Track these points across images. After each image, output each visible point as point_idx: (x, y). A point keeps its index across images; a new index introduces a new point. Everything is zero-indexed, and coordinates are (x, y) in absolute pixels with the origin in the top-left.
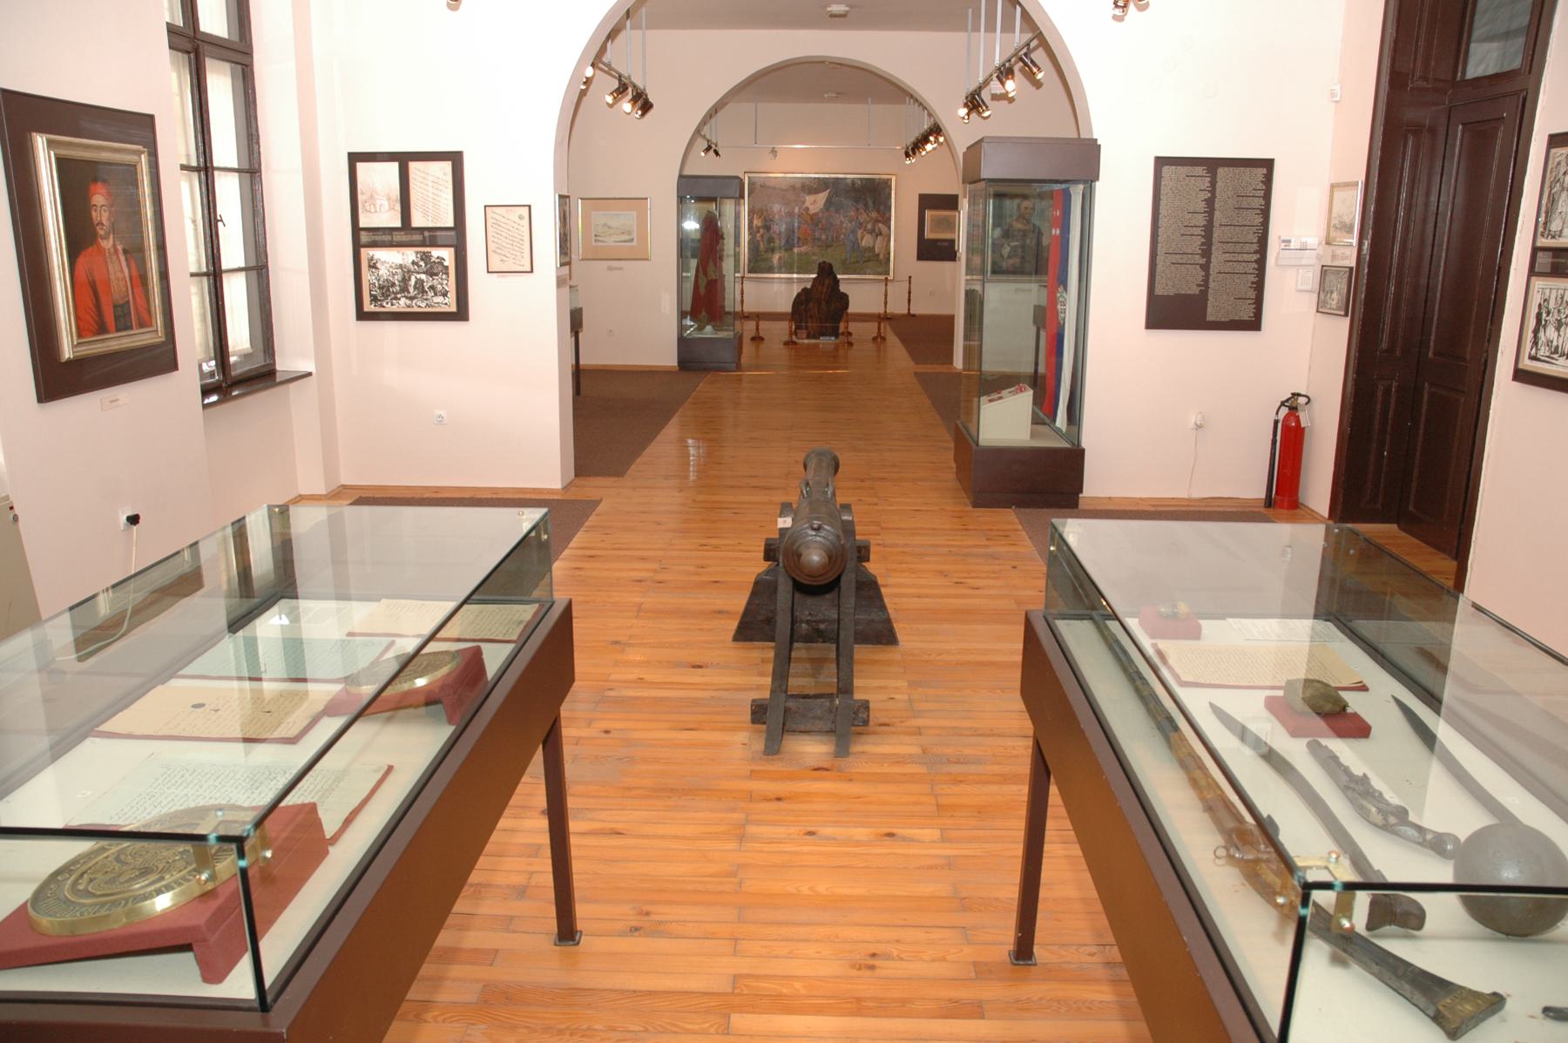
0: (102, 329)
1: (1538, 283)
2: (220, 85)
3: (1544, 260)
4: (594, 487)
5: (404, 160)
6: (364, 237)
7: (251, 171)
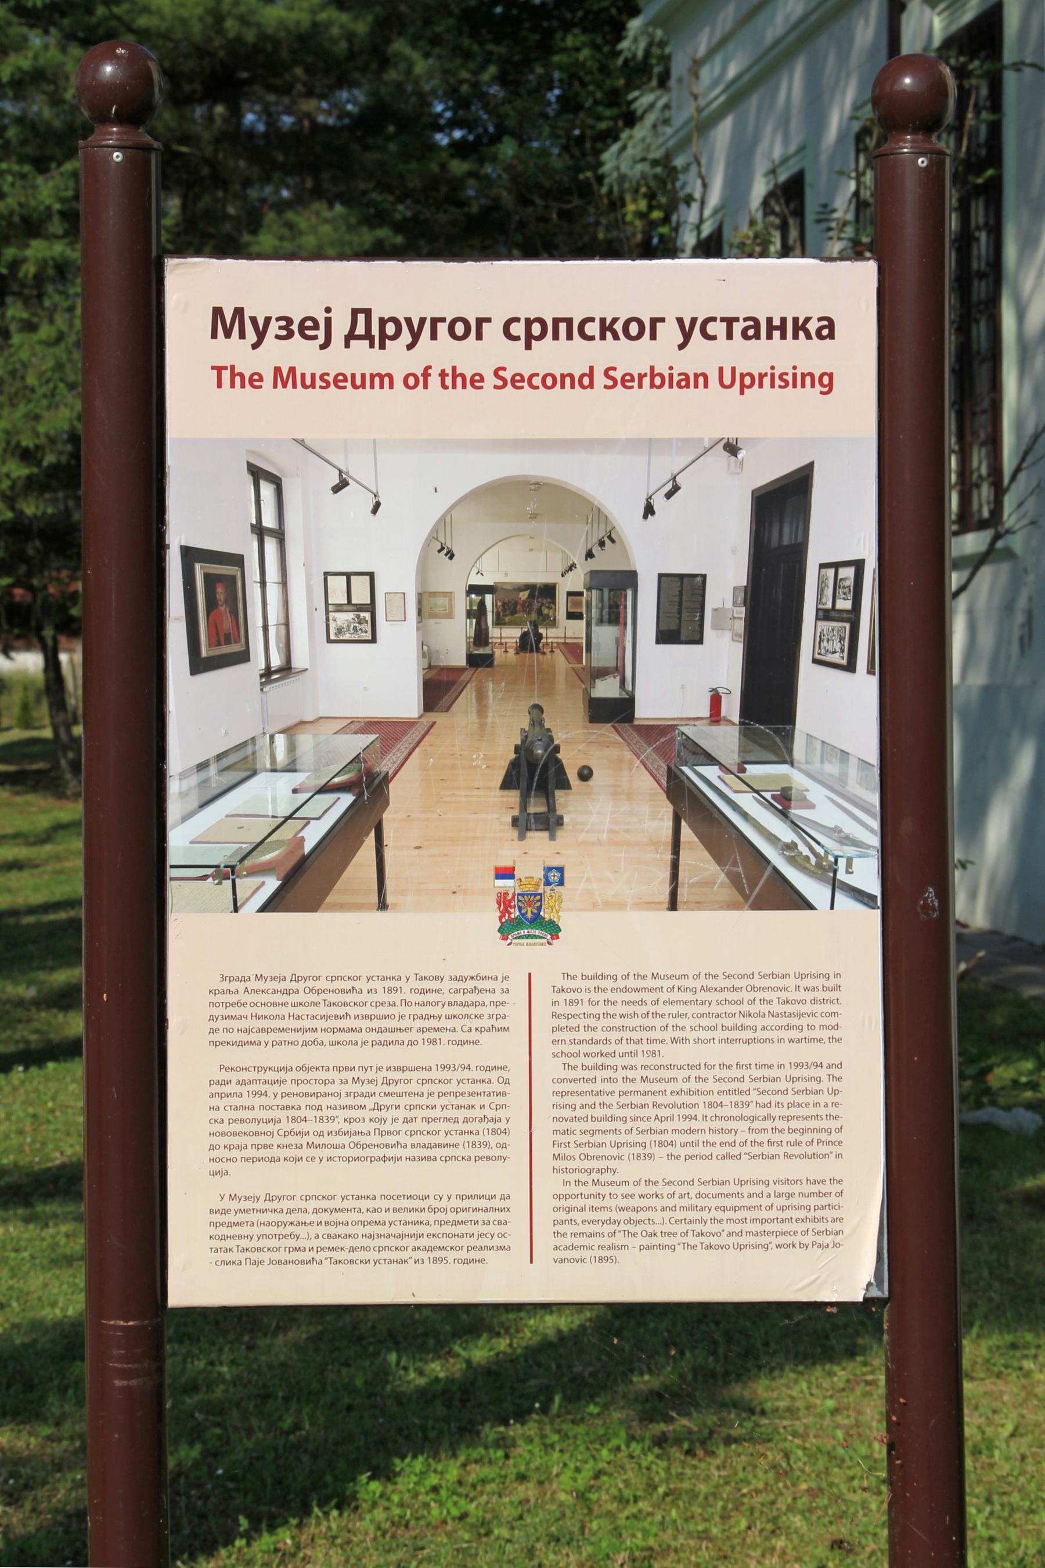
0: (219, 644)
1: (820, 623)
3: (821, 614)
4: (432, 717)
5: (348, 575)
6: (331, 608)
7: (284, 583)
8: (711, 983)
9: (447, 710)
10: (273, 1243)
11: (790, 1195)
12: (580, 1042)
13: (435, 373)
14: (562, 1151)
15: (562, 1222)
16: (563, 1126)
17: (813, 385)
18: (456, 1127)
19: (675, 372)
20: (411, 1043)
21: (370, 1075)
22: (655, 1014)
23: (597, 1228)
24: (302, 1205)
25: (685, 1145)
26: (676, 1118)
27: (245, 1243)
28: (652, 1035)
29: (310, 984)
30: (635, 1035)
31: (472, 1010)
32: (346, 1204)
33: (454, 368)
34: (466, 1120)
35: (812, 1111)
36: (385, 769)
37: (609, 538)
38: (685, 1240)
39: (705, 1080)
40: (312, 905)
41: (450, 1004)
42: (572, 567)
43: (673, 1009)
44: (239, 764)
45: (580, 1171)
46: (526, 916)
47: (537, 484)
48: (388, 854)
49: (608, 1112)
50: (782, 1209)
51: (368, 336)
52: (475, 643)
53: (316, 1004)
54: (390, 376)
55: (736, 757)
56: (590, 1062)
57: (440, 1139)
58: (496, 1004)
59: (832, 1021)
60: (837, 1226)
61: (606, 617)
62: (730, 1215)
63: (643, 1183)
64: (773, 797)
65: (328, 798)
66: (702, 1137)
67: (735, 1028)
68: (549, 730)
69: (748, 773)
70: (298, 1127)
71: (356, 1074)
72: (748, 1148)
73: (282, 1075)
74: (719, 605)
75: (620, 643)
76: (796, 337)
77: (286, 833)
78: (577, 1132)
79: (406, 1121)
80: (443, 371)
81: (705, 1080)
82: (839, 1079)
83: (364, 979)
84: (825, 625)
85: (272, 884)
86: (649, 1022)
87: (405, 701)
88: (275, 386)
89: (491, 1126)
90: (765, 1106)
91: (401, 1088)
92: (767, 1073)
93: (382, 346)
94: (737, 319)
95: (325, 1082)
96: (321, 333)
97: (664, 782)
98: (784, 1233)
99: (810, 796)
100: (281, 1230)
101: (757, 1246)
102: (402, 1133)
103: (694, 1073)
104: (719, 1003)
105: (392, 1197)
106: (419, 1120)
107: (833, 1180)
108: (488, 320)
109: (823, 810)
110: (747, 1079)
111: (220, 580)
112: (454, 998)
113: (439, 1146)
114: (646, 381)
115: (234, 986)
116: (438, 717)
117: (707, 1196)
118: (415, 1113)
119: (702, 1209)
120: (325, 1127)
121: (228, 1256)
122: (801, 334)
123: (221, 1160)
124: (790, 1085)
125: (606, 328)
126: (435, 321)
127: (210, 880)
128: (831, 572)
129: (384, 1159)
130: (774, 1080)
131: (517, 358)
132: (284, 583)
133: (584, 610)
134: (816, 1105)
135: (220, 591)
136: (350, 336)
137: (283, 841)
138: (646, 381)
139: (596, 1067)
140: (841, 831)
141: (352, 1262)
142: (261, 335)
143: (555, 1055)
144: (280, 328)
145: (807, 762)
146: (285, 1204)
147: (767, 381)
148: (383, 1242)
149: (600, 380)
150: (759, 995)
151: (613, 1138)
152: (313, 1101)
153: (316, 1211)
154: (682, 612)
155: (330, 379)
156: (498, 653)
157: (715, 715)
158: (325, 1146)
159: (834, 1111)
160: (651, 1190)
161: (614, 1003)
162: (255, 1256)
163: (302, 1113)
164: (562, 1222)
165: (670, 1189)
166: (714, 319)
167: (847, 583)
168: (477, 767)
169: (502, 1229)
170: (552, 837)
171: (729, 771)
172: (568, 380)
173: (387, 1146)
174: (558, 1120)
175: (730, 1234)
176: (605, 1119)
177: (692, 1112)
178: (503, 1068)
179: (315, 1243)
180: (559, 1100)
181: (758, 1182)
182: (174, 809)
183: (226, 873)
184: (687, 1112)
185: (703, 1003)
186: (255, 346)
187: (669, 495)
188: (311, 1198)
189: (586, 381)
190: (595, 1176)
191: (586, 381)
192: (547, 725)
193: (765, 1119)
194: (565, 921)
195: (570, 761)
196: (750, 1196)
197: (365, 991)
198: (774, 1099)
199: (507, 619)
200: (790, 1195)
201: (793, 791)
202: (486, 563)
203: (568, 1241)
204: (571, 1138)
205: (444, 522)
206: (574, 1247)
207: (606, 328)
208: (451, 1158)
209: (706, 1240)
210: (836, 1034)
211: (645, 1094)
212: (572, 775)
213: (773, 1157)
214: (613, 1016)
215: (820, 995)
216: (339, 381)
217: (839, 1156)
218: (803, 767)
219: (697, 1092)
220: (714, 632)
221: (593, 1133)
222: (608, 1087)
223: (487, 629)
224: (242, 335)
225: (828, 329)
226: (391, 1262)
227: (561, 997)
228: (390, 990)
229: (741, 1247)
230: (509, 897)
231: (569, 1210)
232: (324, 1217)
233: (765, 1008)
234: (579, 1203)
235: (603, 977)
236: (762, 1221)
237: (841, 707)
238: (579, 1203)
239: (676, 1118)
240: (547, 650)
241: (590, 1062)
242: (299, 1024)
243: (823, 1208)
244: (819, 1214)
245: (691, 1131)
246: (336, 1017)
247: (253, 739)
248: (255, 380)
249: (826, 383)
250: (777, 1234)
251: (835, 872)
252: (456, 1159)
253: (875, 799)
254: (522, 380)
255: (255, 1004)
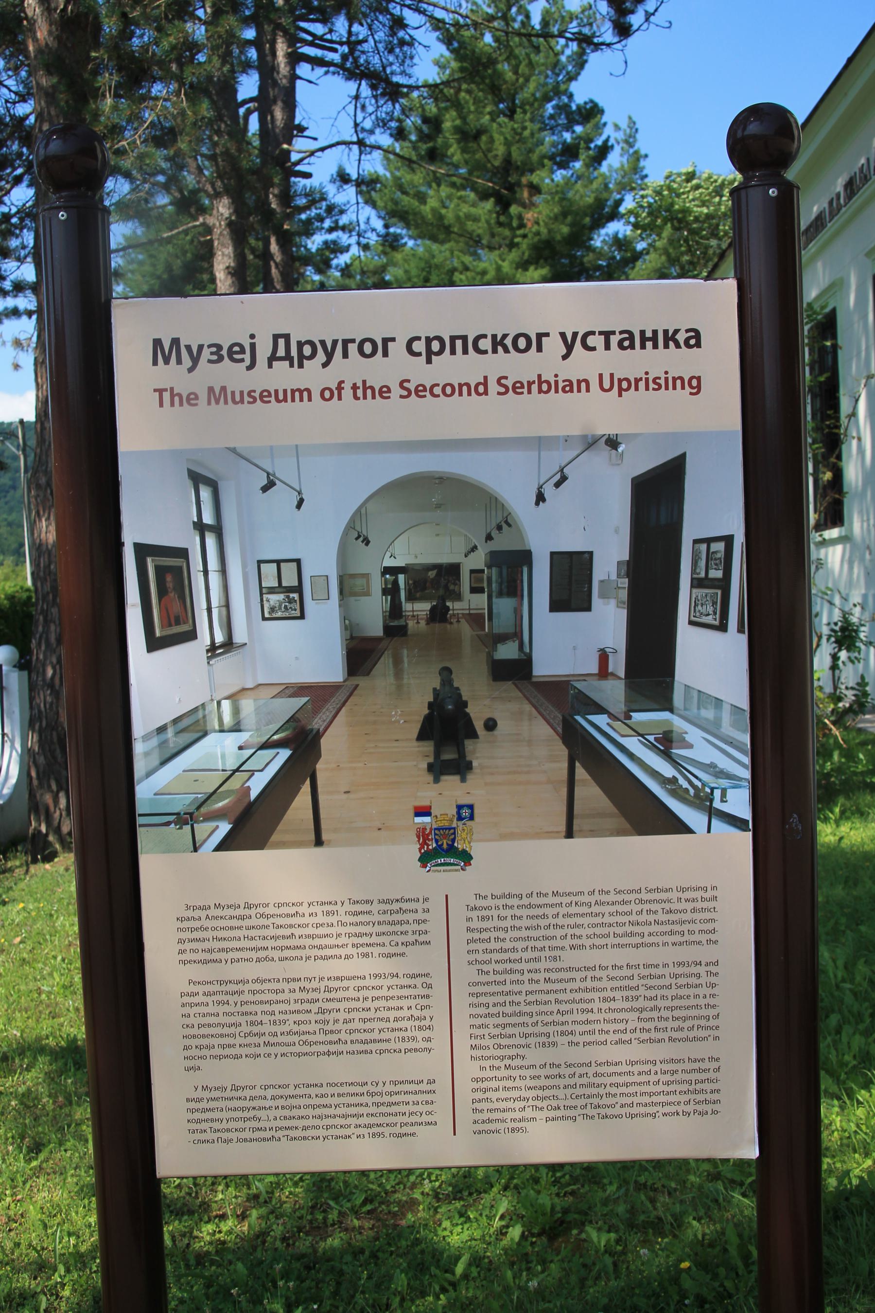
0: (170, 625)
1: (694, 591)
2: (211, 541)
3: (695, 582)
4: (355, 680)
5: (278, 562)
6: (264, 591)
7: (223, 571)
8: (604, 898)
9: (368, 674)
10: (240, 1124)
11: (675, 1072)
12: (491, 951)
13: (347, 386)
14: (478, 1042)
15: (480, 1101)
16: (479, 1021)
17: (683, 388)
18: (388, 1025)
19: (560, 379)
20: (347, 957)
21: (314, 984)
22: (556, 926)
23: (510, 1104)
24: (262, 1093)
25: (583, 1033)
26: (575, 1011)
27: (216, 1125)
28: (554, 943)
29: (261, 910)
30: (539, 944)
31: (398, 928)
32: (299, 1091)
33: (364, 382)
34: (396, 1020)
35: (692, 1002)
36: (316, 727)
37: (506, 522)
38: (584, 1111)
39: (600, 979)
40: (259, 842)
41: (379, 923)
42: (474, 549)
43: (571, 921)
44: (191, 727)
45: (494, 1058)
46: (442, 848)
47: (441, 478)
48: (321, 798)
49: (517, 1009)
50: (667, 1083)
51: (288, 357)
52: (390, 616)
53: (267, 927)
54: (308, 391)
55: (623, 706)
56: (500, 967)
57: (375, 1035)
58: (418, 922)
59: (709, 926)
60: (715, 1097)
61: (505, 590)
62: (623, 1090)
63: (548, 1066)
64: (656, 739)
65: (268, 753)
66: (597, 1027)
67: (626, 935)
68: (458, 689)
69: (633, 720)
70: (255, 1029)
71: (302, 984)
72: (638, 1034)
73: (240, 987)
74: (604, 577)
75: (518, 612)
76: (666, 346)
77: (235, 784)
78: (491, 1026)
79: (345, 1022)
80: (355, 384)
81: (600, 979)
82: (716, 974)
83: (305, 905)
84: (699, 592)
85: (225, 827)
86: (551, 932)
87: (330, 668)
88: (209, 403)
89: (417, 1023)
90: (651, 999)
91: (340, 994)
92: (653, 971)
93: (301, 366)
94: (614, 333)
95: (276, 992)
96: (247, 357)
97: (560, 730)
98: (669, 1104)
99: (688, 738)
100: (246, 1114)
101: (647, 1115)
102: (343, 1032)
103: (590, 974)
104: (611, 914)
105: (336, 1085)
106: (357, 1021)
107: (711, 1059)
108: (393, 340)
109: (700, 748)
110: (636, 977)
111: (169, 571)
112: (382, 918)
113: (375, 1041)
114: (535, 387)
115: (197, 913)
116: (362, 681)
117: (603, 1075)
118: (352, 1015)
119: (599, 1086)
120: (278, 1029)
121: (203, 1137)
122: (671, 344)
123: (194, 1058)
124: (673, 981)
125: (498, 343)
126: (346, 342)
127: (173, 825)
128: (704, 547)
129: (329, 1053)
130: (659, 977)
131: (419, 371)
132: (223, 571)
133: (485, 585)
134: (696, 996)
135: (169, 578)
136: (273, 358)
137: (232, 791)
138: (535, 387)
139: (505, 972)
140: (716, 766)
141: (305, 1138)
142: (195, 360)
143: (470, 963)
144: (212, 353)
145: (685, 709)
146: (248, 1093)
147: (642, 385)
148: (330, 1121)
149: (493, 387)
150: (646, 907)
151: (522, 1029)
152: (266, 1008)
153: (273, 1098)
154: (572, 582)
155: (257, 395)
156: (411, 624)
157: (604, 672)
158: (279, 1044)
159: (712, 1001)
160: (555, 1071)
161: (520, 918)
162: (225, 1136)
163: (258, 1018)
164: (480, 1101)
165: (571, 1071)
166: (593, 333)
167: (719, 555)
168: (395, 722)
169: (429, 1108)
170: (463, 780)
171: (616, 719)
172: (465, 388)
173: (330, 1043)
174: (474, 1016)
175: (622, 1106)
176: (514, 1014)
177: (589, 1006)
178: (427, 975)
179: (274, 1124)
180: (474, 1000)
181: (647, 1062)
182: (140, 766)
183: (185, 819)
184: (585, 1006)
185: (597, 915)
186: (191, 370)
187: (558, 485)
188: (269, 1087)
189: (481, 389)
190: (507, 1062)
191: (481, 389)
192: (456, 685)
193: (651, 1010)
194: (477, 850)
195: (477, 713)
196: (640, 1074)
197: (307, 915)
198: (660, 993)
199: (418, 595)
200: (675, 1072)
201: (674, 734)
202: (399, 547)
203: (485, 1116)
204: (485, 1031)
205: (359, 514)
206: (490, 1121)
207: (498, 343)
208: (384, 1051)
209: (602, 1111)
210: (713, 937)
211: (548, 992)
212: (479, 725)
213: (659, 1041)
214: (520, 928)
215: (699, 905)
216: (264, 396)
217: (716, 1038)
218: (682, 713)
219: (593, 989)
220: (601, 601)
221: (504, 1026)
222: (516, 988)
223: (401, 603)
224: (179, 361)
225: (695, 339)
226: (337, 1137)
227: (474, 914)
228: (328, 913)
229: (632, 1116)
230: (428, 831)
231: (485, 1090)
232: (281, 1102)
233: (651, 918)
234: (494, 1084)
235: (510, 896)
236: (650, 1094)
237: (713, 661)
238: (494, 1084)
239: (575, 1011)
240: (454, 620)
241: (500, 967)
242: (253, 944)
243: (702, 1082)
244: (699, 1087)
245: (588, 1022)
246: (284, 937)
247: (203, 704)
248: (192, 399)
249: (695, 385)
250: (663, 1104)
251: (711, 801)
252: (389, 1051)
253: (746, 739)
254: (425, 390)
255: (216, 929)
